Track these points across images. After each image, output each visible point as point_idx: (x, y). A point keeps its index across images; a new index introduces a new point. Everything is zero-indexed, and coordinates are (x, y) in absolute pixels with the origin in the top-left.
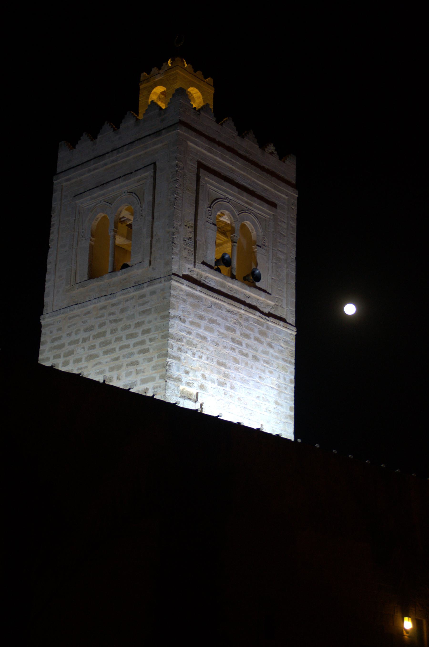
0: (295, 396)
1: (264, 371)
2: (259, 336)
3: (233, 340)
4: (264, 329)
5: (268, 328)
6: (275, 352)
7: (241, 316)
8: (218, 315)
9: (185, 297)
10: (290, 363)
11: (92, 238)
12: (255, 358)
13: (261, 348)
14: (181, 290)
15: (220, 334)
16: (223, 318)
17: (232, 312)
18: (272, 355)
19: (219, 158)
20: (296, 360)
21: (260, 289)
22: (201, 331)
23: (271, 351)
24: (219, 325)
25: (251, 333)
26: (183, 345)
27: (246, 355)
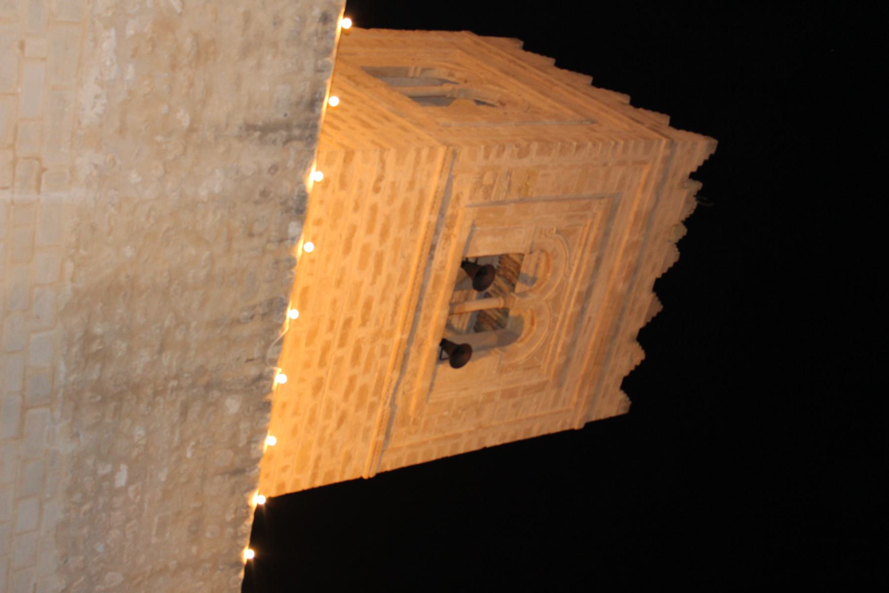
0: (641, 100)
1: (295, 413)
2: (357, 388)
3: (348, 323)
4: (370, 398)
5: (373, 407)
6: (331, 435)
7: (391, 334)
8: (389, 278)
9: (417, 186)
10: (314, 476)
11: (419, 69)
12: (318, 387)
13: (337, 397)
14: (429, 175)
15: (359, 285)
16: (385, 290)
17: (395, 312)
18: (324, 429)
19: (628, 241)
20: (321, 489)
21: (434, 374)
22: (360, 238)
23: (333, 423)
24: (373, 283)
25: (363, 365)
26: (333, 191)
27: (322, 363)
